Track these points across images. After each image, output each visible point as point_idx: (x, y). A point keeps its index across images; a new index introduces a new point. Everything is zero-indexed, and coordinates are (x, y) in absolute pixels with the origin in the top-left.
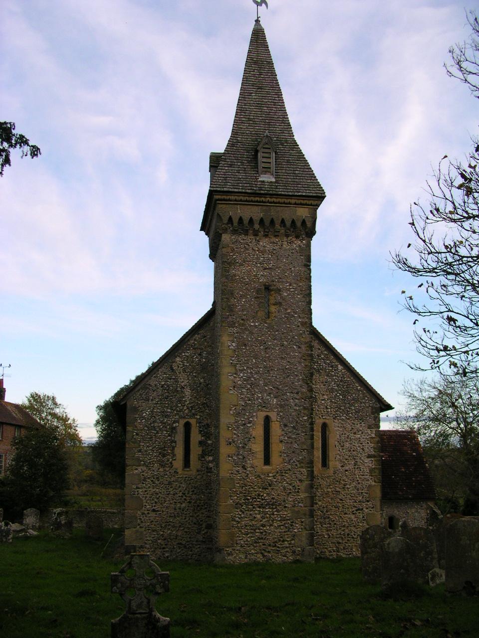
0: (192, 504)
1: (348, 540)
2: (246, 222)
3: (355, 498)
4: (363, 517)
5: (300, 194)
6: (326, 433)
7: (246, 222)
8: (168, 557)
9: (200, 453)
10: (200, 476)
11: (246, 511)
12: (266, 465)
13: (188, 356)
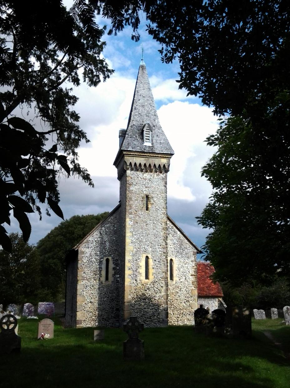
1: (182, 316)
2: (138, 165)
3: (186, 295)
5: (163, 152)
6: (172, 264)
7: (138, 165)
9: (113, 273)
10: (113, 285)
11: (137, 301)
12: (146, 279)
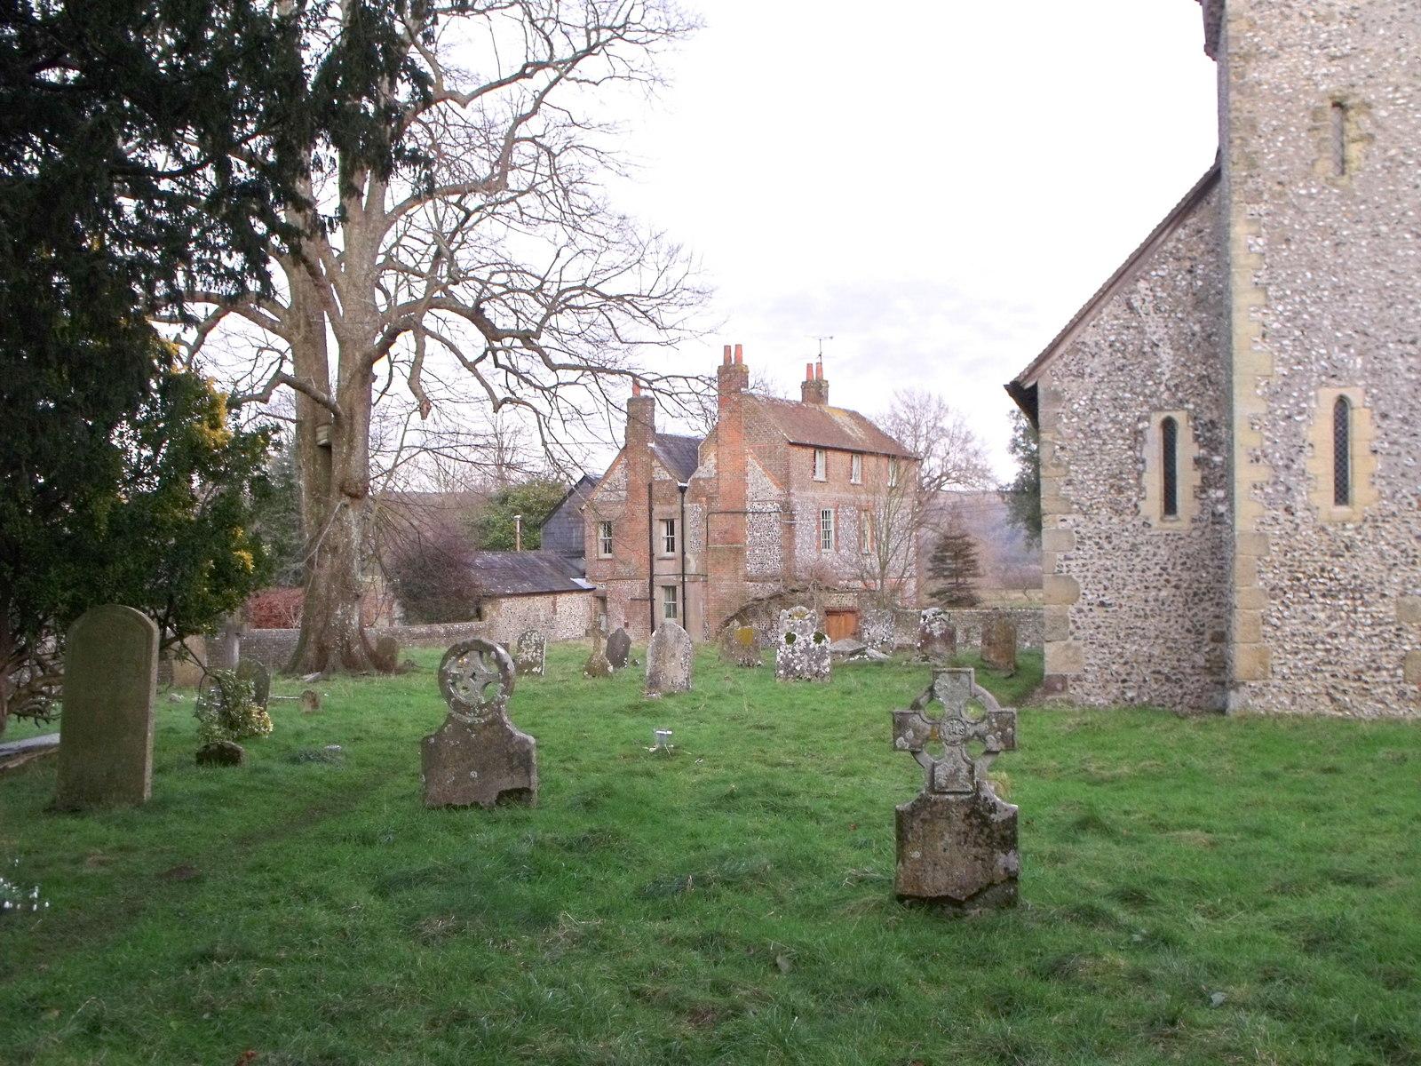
0: (1182, 590)
8: (1132, 699)
9: (1198, 483)
13: (1162, 277)
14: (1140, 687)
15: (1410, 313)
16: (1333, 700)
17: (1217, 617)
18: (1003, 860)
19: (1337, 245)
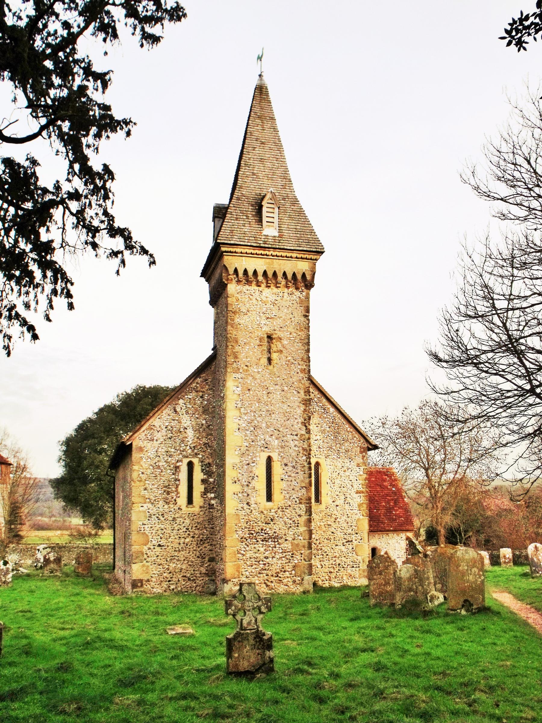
0: (196, 539)
2: (250, 273)
4: (353, 548)
6: (318, 471)
8: (173, 589)
9: (203, 490)
13: (190, 399)
14: (177, 584)
15: (295, 423)
16: (267, 586)
17: (211, 550)
18: (268, 653)
19: (268, 393)
